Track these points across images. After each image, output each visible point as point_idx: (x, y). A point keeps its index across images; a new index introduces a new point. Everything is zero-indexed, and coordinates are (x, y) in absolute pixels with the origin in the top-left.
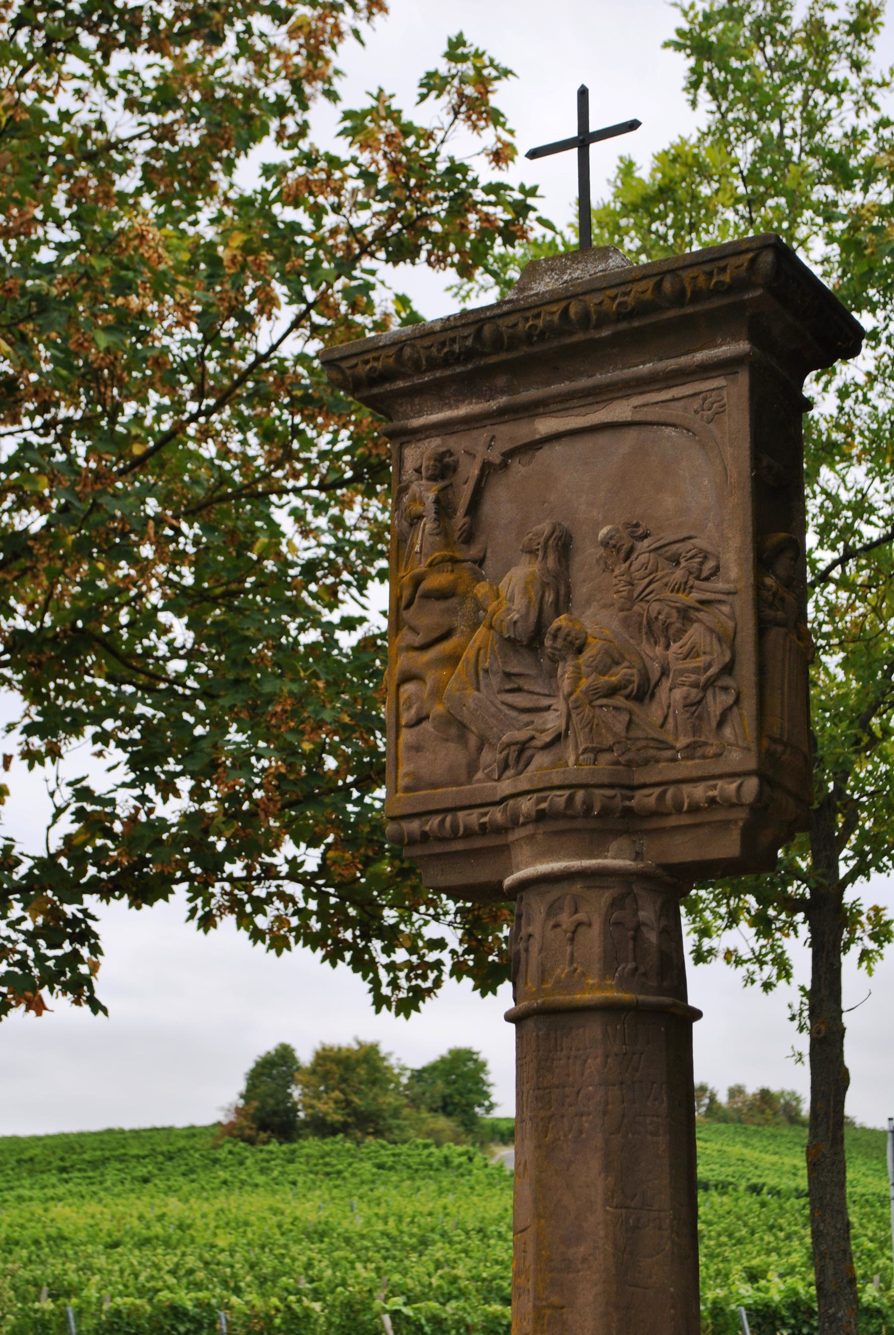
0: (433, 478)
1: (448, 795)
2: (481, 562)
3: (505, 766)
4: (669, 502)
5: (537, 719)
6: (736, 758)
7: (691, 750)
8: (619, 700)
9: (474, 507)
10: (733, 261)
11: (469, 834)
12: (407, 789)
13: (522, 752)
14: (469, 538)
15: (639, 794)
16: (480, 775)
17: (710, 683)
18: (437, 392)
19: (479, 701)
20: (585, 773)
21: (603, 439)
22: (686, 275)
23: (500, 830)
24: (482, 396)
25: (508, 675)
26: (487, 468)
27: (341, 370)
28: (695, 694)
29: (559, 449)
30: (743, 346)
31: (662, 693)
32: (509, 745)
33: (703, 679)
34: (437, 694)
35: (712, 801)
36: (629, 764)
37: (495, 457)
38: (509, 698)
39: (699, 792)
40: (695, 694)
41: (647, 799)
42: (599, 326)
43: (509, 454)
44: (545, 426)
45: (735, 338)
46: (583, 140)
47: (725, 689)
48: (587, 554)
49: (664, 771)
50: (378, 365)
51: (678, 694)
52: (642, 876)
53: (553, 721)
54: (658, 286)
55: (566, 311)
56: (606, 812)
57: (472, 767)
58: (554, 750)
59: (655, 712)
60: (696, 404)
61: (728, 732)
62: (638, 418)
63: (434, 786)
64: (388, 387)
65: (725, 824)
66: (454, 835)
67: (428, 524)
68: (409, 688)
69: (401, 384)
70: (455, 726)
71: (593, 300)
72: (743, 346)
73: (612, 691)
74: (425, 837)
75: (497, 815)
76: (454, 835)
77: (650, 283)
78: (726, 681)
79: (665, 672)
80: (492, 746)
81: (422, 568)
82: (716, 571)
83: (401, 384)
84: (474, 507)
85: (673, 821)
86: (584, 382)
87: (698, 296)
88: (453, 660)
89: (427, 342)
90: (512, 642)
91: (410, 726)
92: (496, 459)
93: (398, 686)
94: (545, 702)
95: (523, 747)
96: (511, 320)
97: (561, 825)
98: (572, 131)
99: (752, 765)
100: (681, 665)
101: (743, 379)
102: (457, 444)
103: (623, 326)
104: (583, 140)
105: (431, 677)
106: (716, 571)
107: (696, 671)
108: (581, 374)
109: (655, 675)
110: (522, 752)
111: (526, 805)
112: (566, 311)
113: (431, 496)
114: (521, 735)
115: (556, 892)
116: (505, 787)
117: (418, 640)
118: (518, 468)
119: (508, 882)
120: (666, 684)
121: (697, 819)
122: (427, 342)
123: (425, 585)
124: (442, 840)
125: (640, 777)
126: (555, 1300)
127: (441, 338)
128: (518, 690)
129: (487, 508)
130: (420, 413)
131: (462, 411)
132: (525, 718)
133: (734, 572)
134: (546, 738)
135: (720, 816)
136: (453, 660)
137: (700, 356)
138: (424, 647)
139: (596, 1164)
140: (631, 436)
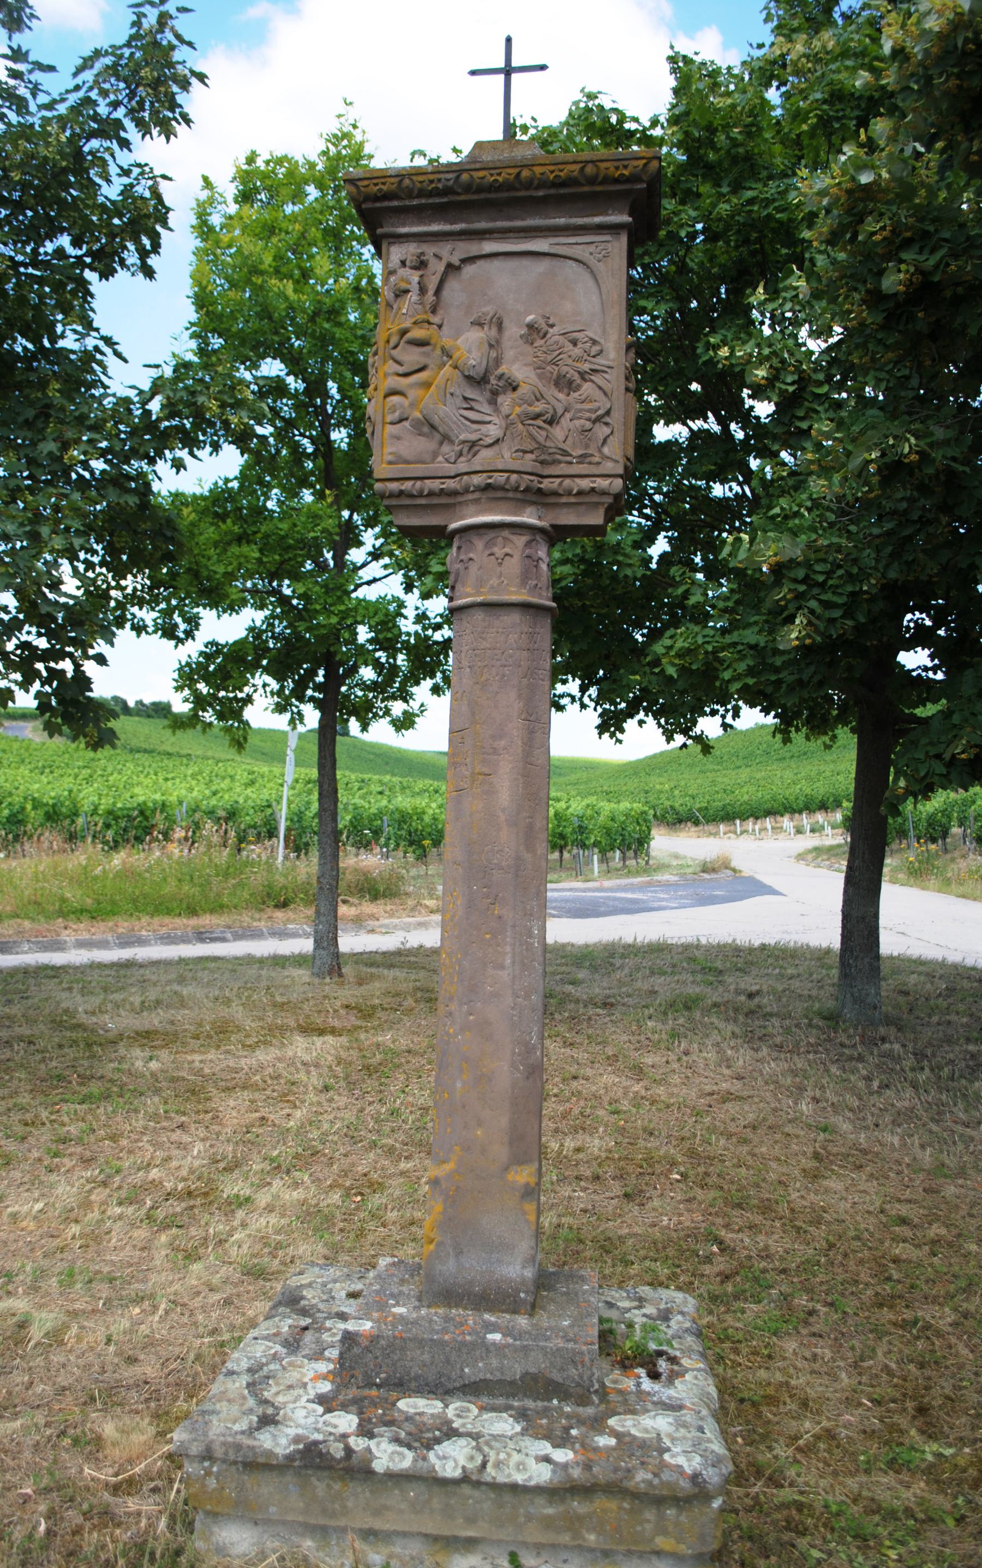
0: (415, 268)
1: (418, 470)
2: (440, 326)
3: (461, 454)
4: (568, 306)
5: (484, 428)
6: (609, 467)
7: (583, 458)
8: (539, 422)
9: (438, 292)
10: (636, 163)
11: (431, 494)
12: (390, 463)
13: (473, 446)
14: (434, 311)
15: (546, 481)
16: (440, 458)
17: (598, 420)
18: (419, 213)
19: (448, 413)
20: (516, 466)
21: (525, 262)
22: (603, 165)
23: (455, 493)
24: (447, 221)
25: (465, 399)
26: (450, 266)
27: (357, 187)
28: (588, 425)
29: (497, 263)
30: (626, 218)
31: (565, 422)
32: (464, 442)
33: (594, 416)
34: (413, 405)
35: (593, 489)
36: (542, 462)
37: (455, 261)
38: (466, 413)
39: (585, 484)
40: (588, 425)
41: (546, 484)
42: (538, 187)
43: (464, 261)
44: (489, 247)
45: (621, 212)
46: (508, 71)
47: (607, 424)
48: (514, 331)
49: (562, 469)
50: (385, 188)
51: (578, 423)
52: (541, 530)
53: (494, 431)
54: (582, 169)
55: (519, 174)
56: (527, 490)
57: (435, 455)
58: (496, 448)
59: (558, 432)
60: (592, 248)
61: (606, 450)
62: (552, 251)
63: (408, 462)
64: (386, 204)
65: (596, 505)
66: (421, 495)
67: (413, 296)
68: (395, 399)
69: (395, 203)
70: (428, 426)
71: (538, 170)
72: (626, 218)
73: (537, 416)
74: (401, 493)
75: (451, 484)
76: (421, 495)
77: (577, 167)
78: (607, 419)
79: (566, 410)
80: (452, 442)
81: (407, 324)
82: (601, 352)
83: (395, 203)
84: (438, 292)
85: (564, 500)
86: (518, 223)
87: (607, 180)
88: (427, 385)
89: (421, 178)
90: (469, 378)
91: (392, 423)
92: (456, 262)
93: (386, 396)
94: (488, 418)
95: (473, 444)
96: (481, 174)
97: (500, 494)
98: (501, 64)
99: (621, 471)
100: (579, 406)
101: (624, 239)
102: (429, 250)
103: (552, 191)
104: (508, 71)
105: (412, 394)
106: (601, 352)
107: (589, 411)
108: (516, 218)
109: (560, 412)
110: (473, 446)
111: (477, 480)
112: (519, 174)
113: (416, 279)
114: (473, 437)
115: (492, 534)
116: (462, 466)
117: (401, 370)
118: (469, 270)
119: (453, 526)
120: (568, 416)
121: (580, 500)
122: (421, 178)
123: (409, 336)
124: (411, 496)
125: (546, 472)
126: (485, 770)
127: (431, 177)
128: (471, 409)
129: (445, 293)
130: (404, 225)
131: (435, 227)
132: (475, 426)
133: (612, 355)
134: (489, 441)
135: (595, 499)
136: (427, 385)
137: (597, 220)
138: (406, 375)
139: (513, 694)
140: (543, 266)
